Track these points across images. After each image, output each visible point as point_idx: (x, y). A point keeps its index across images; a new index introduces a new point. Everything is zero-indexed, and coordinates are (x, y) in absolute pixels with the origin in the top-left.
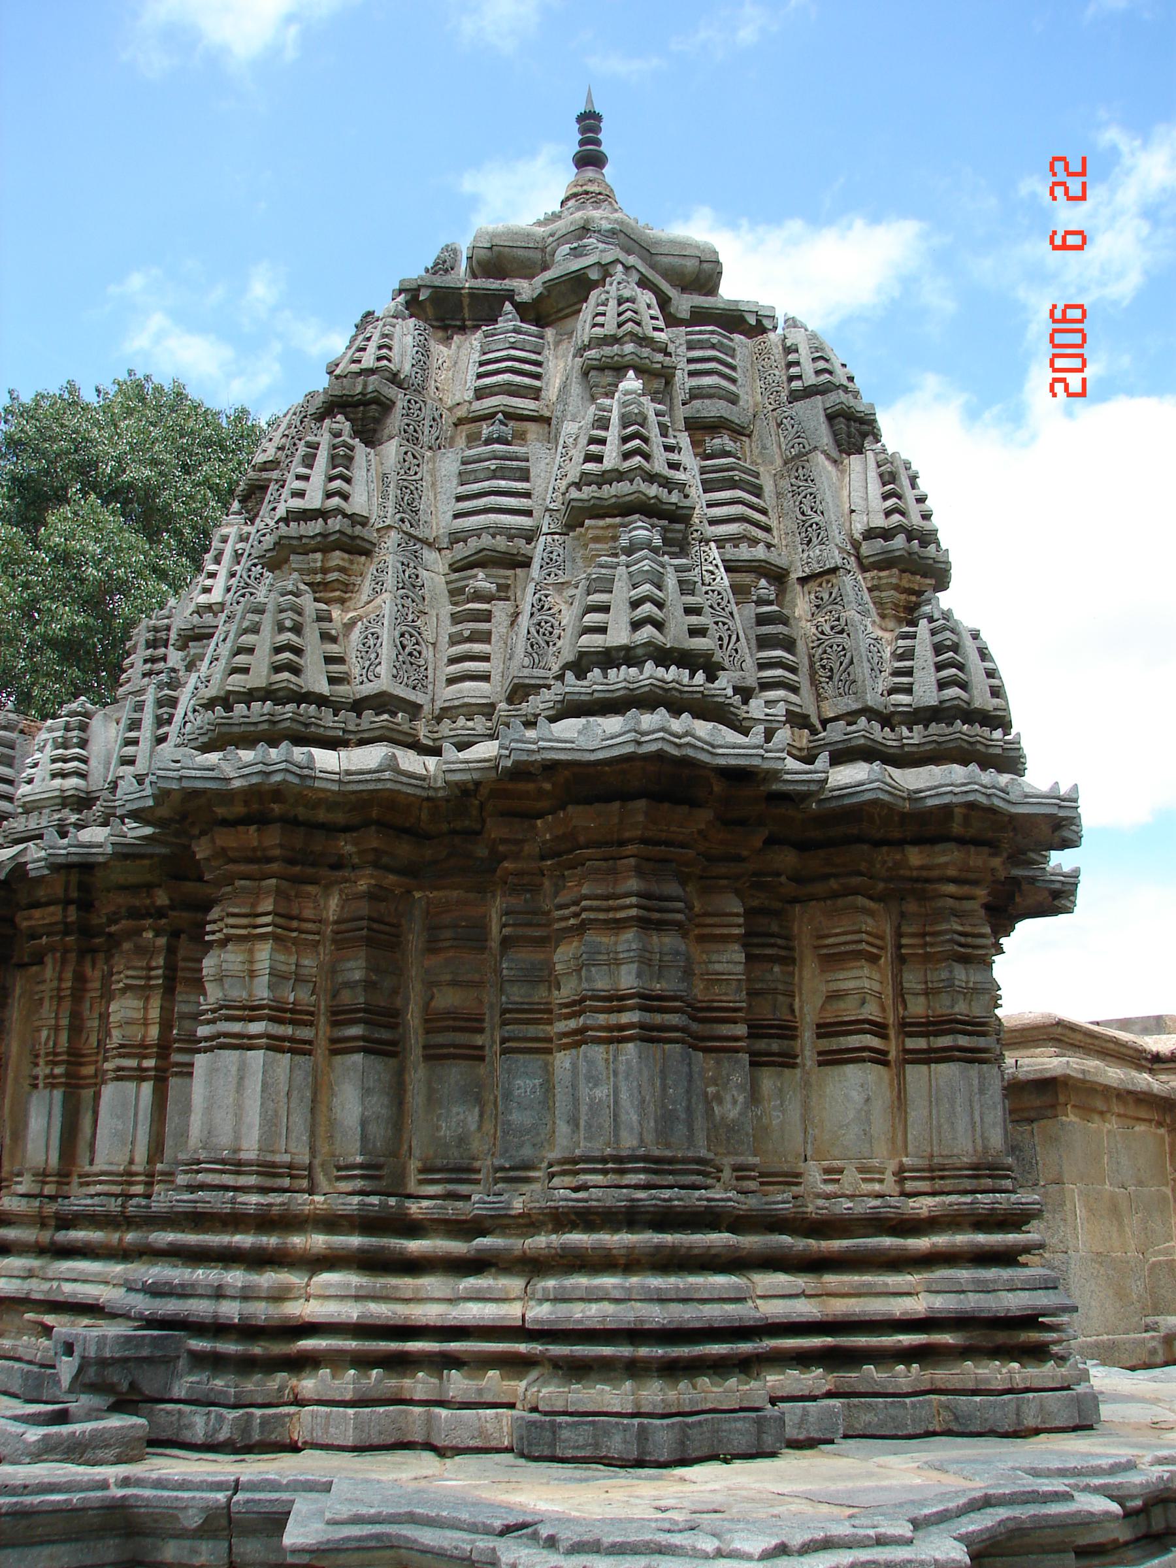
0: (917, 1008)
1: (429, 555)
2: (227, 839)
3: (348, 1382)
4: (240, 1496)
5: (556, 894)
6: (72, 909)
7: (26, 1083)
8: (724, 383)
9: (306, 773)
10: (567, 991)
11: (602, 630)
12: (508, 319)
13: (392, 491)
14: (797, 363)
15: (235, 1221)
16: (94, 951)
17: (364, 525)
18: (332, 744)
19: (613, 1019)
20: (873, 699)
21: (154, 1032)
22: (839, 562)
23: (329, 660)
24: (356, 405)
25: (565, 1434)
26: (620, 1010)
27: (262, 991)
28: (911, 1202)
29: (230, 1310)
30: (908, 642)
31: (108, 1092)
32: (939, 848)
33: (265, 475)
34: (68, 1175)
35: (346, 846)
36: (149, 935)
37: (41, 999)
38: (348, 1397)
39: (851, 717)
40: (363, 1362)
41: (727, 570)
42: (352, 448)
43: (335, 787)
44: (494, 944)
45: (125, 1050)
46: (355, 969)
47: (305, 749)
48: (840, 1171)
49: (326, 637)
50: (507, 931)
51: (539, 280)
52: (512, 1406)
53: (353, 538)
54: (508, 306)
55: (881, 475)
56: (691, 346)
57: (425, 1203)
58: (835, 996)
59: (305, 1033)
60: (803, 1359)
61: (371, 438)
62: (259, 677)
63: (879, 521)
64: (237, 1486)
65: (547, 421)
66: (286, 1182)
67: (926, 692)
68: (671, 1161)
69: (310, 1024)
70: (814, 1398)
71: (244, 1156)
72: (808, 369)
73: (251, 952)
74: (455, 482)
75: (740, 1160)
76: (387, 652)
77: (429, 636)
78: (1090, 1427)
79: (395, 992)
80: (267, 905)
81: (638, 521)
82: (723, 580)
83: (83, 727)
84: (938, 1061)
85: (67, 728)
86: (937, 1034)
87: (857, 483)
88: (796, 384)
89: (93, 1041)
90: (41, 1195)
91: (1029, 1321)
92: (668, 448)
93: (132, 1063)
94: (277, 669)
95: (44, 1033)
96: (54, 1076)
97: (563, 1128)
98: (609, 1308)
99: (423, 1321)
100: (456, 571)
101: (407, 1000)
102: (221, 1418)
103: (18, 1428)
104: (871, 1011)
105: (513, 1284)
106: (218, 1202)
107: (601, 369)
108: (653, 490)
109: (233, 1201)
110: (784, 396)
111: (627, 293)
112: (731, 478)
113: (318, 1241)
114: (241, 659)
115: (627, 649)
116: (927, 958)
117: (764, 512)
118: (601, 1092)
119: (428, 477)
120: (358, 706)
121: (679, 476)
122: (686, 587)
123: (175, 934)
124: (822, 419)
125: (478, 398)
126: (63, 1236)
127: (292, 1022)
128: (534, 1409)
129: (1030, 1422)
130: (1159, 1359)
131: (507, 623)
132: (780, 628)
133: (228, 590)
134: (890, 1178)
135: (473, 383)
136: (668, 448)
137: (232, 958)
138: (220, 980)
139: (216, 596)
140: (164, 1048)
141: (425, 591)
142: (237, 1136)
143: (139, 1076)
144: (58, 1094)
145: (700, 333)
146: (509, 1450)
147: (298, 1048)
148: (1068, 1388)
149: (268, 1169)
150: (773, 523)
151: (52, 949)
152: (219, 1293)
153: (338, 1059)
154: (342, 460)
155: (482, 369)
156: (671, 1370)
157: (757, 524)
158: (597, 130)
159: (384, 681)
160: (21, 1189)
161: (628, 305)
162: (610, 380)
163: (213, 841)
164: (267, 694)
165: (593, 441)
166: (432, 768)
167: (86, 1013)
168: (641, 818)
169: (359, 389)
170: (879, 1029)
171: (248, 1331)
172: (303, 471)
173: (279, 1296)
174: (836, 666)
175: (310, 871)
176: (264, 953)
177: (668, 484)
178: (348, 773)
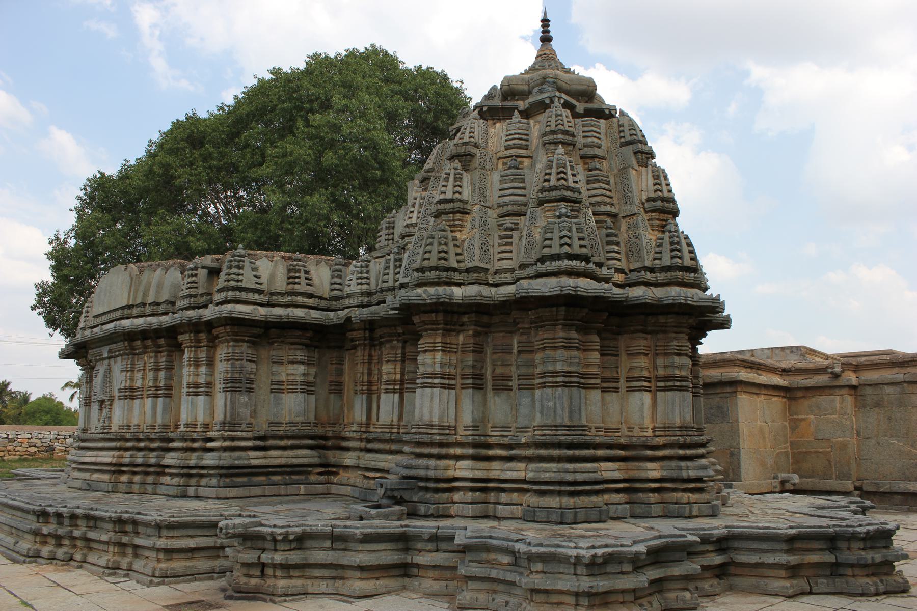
0: (661, 372)
1: (490, 211)
2: (425, 317)
3: (469, 496)
4: (439, 531)
5: (536, 336)
6: (367, 332)
7: (352, 392)
8: (596, 140)
9: (451, 297)
10: (539, 370)
11: (550, 247)
12: (516, 117)
13: (477, 190)
14: (623, 131)
15: (431, 444)
16: (374, 346)
17: (467, 203)
18: (458, 285)
19: (555, 379)
20: (648, 263)
21: (398, 377)
22: (636, 211)
23: (457, 254)
24: (462, 156)
25: (538, 514)
26: (557, 376)
27: (438, 369)
28: (657, 439)
29: (431, 474)
30: (661, 241)
31: (383, 396)
32: (669, 316)
33: (429, 174)
34: (369, 424)
35: (465, 319)
36: (395, 342)
37: (357, 363)
38: (469, 501)
39: (638, 270)
40: (473, 490)
41: (594, 215)
42: (461, 174)
43: (461, 302)
44: (515, 351)
45: (387, 383)
46: (470, 359)
47: (449, 288)
48: (633, 428)
49: (455, 246)
50: (519, 349)
51: (527, 102)
52: (521, 504)
53: (464, 209)
54: (516, 112)
55: (653, 176)
56: (583, 126)
57: (494, 438)
58: (632, 368)
59: (453, 382)
60: (618, 491)
61: (466, 168)
62: (434, 262)
63: (652, 195)
64: (438, 528)
65: (531, 157)
66: (447, 432)
67: (667, 261)
68: (574, 426)
69: (454, 379)
70: (620, 504)
71: (433, 423)
72: (627, 133)
73: (434, 355)
74: (498, 184)
75: (598, 425)
76: (477, 251)
77: (491, 243)
78: (716, 516)
79: (482, 367)
80: (439, 340)
81: (563, 204)
82: (593, 224)
83: (367, 266)
84: (668, 390)
85: (362, 267)
86: (668, 381)
87: (644, 180)
88: (622, 140)
89: (376, 378)
90: (360, 431)
91: (699, 480)
92: (574, 175)
93: (391, 387)
94: (440, 259)
95: (359, 375)
96: (362, 390)
97: (538, 415)
98: (553, 474)
99: (493, 477)
100: (500, 217)
101: (487, 369)
102: (429, 508)
103: (368, 510)
104: (645, 373)
105: (522, 465)
106: (426, 439)
107: (550, 143)
108: (569, 193)
109: (431, 438)
110: (618, 145)
111: (559, 113)
112: (598, 179)
113: (459, 451)
114: (427, 255)
115: (558, 254)
116: (666, 354)
117: (610, 191)
118: (550, 404)
119: (489, 183)
120: (468, 271)
121: (577, 186)
122: (579, 230)
123: (405, 342)
124: (632, 154)
125: (506, 149)
126: (370, 446)
127: (448, 379)
128: (529, 506)
129: (694, 513)
130: (778, 490)
131: (518, 239)
132: (616, 239)
133: (418, 218)
134: (650, 431)
135: (504, 144)
136: (574, 175)
137: (428, 357)
138: (424, 364)
139: (414, 220)
140: (402, 382)
141: (489, 226)
142: (431, 417)
143: (394, 391)
144: (365, 396)
145: (587, 120)
146: (520, 519)
147: (450, 387)
148: (709, 503)
149: (441, 427)
150: (614, 195)
151: (360, 345)
152: (427, 468)
153: (463, 390)
154: (458, 178)
155: (507, 138)
156: (572, 494)
157: (607, 196)
158: (548, 26)
159: (476, 263)
160: (353, 429)
161: (559, 117)
162: (553, 147)
163: (420, 318)
164: (436, 269)
165: (546, 174)
166: (493, 293)
167: (373, 368)
168: (563, 313)
169: (463, 150)
170: (648, 380)
171: (437, 480)
172: (445, 184)
173: (447, 469)
174: (634, 250)
175: (453, 327)
176: (439, 356)
177: (572, 190)
178: (465, 297)
